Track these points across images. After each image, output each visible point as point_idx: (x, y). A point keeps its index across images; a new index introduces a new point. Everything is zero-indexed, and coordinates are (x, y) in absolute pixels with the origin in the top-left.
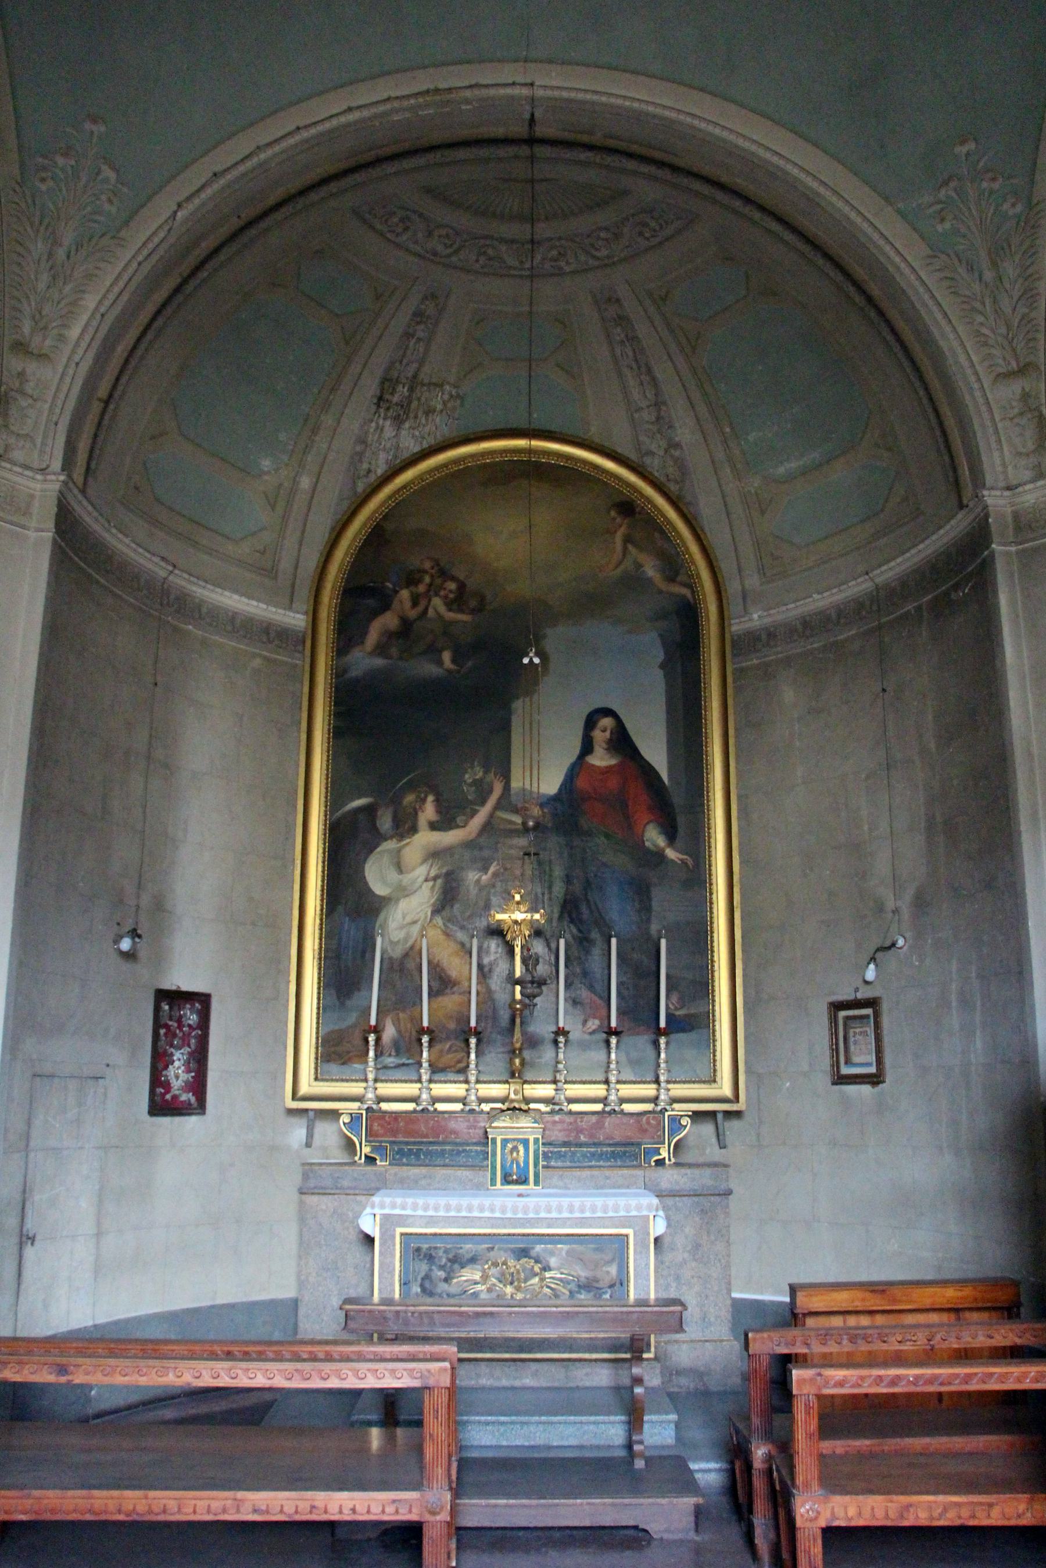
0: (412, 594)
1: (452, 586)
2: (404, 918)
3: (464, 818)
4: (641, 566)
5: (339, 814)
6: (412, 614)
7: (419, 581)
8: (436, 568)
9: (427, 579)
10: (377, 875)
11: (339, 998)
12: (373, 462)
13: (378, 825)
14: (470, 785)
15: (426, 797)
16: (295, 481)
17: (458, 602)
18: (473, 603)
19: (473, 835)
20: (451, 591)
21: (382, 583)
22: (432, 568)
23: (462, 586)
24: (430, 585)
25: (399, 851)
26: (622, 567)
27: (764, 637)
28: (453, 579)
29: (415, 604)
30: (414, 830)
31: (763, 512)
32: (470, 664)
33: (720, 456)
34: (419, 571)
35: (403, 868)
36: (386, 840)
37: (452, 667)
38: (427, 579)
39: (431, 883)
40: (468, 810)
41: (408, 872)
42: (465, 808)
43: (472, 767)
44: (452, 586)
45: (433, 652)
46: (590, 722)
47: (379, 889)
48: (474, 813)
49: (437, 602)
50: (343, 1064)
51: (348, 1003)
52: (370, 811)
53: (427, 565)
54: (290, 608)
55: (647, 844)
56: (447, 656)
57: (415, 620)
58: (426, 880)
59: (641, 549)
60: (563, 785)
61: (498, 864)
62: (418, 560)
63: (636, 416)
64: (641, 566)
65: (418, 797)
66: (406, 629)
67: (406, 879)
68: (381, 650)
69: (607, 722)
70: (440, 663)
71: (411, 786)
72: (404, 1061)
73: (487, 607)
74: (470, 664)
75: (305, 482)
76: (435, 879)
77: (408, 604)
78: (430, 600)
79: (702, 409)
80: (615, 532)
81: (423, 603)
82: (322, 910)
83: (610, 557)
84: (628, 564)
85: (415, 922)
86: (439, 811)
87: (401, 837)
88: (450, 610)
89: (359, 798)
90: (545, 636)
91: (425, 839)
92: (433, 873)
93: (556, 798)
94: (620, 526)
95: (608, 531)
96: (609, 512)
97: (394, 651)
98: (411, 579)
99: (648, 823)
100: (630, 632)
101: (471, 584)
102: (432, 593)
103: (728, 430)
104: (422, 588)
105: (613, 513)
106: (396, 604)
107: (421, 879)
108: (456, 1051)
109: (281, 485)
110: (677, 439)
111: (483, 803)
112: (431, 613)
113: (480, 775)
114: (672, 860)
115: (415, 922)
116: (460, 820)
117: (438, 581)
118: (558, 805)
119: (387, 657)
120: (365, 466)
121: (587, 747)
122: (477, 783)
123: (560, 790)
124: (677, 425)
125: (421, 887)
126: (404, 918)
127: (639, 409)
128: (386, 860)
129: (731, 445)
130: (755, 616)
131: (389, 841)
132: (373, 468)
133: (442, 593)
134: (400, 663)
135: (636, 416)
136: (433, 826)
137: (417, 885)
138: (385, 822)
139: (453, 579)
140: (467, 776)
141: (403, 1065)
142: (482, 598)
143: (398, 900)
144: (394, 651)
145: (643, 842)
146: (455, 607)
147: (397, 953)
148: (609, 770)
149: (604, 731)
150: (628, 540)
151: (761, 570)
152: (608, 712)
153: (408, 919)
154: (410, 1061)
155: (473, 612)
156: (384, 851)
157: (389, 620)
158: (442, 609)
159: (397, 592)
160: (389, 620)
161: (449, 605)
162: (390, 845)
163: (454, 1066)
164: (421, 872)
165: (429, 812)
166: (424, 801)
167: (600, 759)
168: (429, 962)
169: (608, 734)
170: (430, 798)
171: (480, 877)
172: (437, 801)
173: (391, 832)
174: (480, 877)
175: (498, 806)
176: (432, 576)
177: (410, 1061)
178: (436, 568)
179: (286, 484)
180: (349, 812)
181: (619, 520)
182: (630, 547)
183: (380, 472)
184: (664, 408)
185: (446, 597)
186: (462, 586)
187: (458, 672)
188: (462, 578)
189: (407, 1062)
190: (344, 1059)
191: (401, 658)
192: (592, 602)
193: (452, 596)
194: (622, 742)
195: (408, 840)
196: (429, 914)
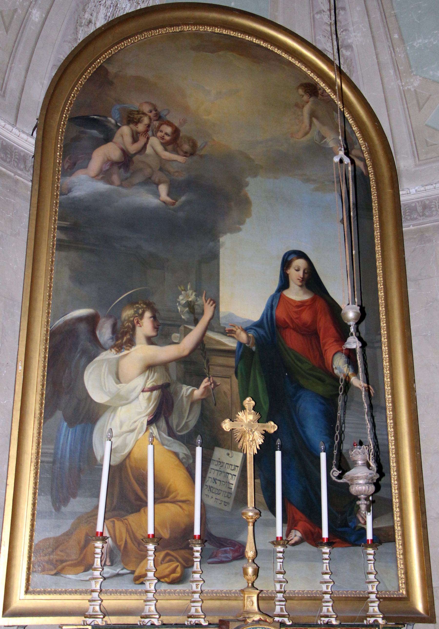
0: (132, 131)
1: (169, 130)
2: (121, 427)
3: (178, 335)
4: (323, 138)
5: (60, 321)
6: (132, 148)
7: (139, 121)
8: (154, 112)
9: (146, 120)
10: (96, 382)
11: (54, 504)
12: (95, 14)
13: (97, 333)
14: (184, 306)
15: (143, 313)
16: (27, 12)
17: (174, 142)
18: (186, 147)
19: (186, 353)
20: (166, 134)
21: (106, 117)
22: (151, 112)
23: (176, 131)
24: (149, 126)
25: (118, 361)
26: (309, 136)
27: (419, 209)
28: (169, 124)
29: (135, 140)
30: (131, 343)
31: (420, 108)
32: (183, 198)
33: (385, 57)
34: (138, 112)
35: (122, 379)
36: (106, 350)
37: (168, 199)
38: (146, 120)
39: (148, 394)
40: (182, 328)
41: (127, 382)
42: (179, 326)
43: (185, 290)
44: (169, 130)
45: (150, 183)
46: (286, 263)
47: (98, 396)
48: (187, 331)
49: (155, 142)
50: (56, 574)
51: (63, 509)
52: (92, 321)
53: (146, 108)
54: (14, 125)
55: (336, 371)
56: (163, 189)
57: (136, 154)
58: (143, 391)
59: (323, 123)
60: (265, 315)
61: (209, 380)
62: (136, 102)
63: (318, 17)
64: (323, 138)
65: (136, 312)
66: (126, 161)
67: (124, 388)
68: (104, 175)
69: (300, 263)
70: (157, 195)
71: (131, 302)
72: (118, 570)
73: (198, 153)
74: (183, 198)
75: (36, 15)
76: (152, 390)
77: (128, 139)
78: (148, 139)
79: (376, 16)
80: (303, 107)
81: (142, 141)
82: (41, 414)
83: (297, 126)
84: (313, 135)
85: (132, 431)
86: (156, 328)
87: (119, 348)
88: (166, 150)
89: (85, 307)
90: (247, 184)
91: (142, 352)
92: (149, 385)
93: (259, 325)
94: (307, 102)
95: (296, 105)
96: (297, 91)
97: (115, 178)
98: (132, 118)
99: (336, 353)
100: (317, 189)
101: (184, 131)
102: (150, 133)
103: (396, 36)
104: (141, 127)
105: (301, 91)
106: (117, 138)
107: (140, 388)
108: (170, 561)
109: (15, 11)
110: (349, 41)
111: (196, 322)
112: (149, 150)
113: (192, 298)
114: (358, 388)
115: (132, 431)
116: (175, 336)
117: (156, 123)
118: (261, 332)
119: (110, 182)
120: (87, 16)
121: (285, 283)
122: (190, 306)
123: (262, 319)
124: (351, 29)
125: (137, 397)
126: (121, 427)
127: (321, 12)
128: (105, 369)
129: (397, 50)
130: (413, 191)
131: (108, 351)
132: (93, 19)
133: (159, 134)
134: (120, 189)
135: (318, 17)
136: (150, 341)
137: (134, 394)
138: (105, 333)
139: (169, 124)
140: (181, 297)
141: (118, 575)
142: (194, 145)
143: (115, 409)
144: (115, 178)
145: (333, 369)
146: (170, 147)
147: (117, 460)
148: (302, 304)
149: (298, 270)
150: (313, 115)
151: (416, 154)
152: (301, 255)
153: (125, 428)
154: (125, 571)
155: (185, 154)
156: (103, 361)
157: (110, 151)
158: (160, 148)
159: (119, 127)
160: (110, 151)
161: (165, 145)
162: (108, 355)
163: (167, 576)
164: (139, 382)
165: (146, 327)
166: (141, 316)
167: (296, 294)
168: (134, 477)
169: (301, 273)
170: (148, 314)
171: (193, 391)
172: (154, 317)
173: (110, 343)
174: (193, 391)
175: (209, 327)
176: (150, 119)
177: (125, 571)
178: (154, 112)
179: (19, 11)
180: (71, 320)
181: (306, 98)
182: (314, 120)
183: (99, 25)
184: (342, 13)
185: (162, 138)
186: (176, 131)
187: (173, 204)
188: (177, 124)
189: (122, 572)
190: (58, 568)
191: (121, 185)
192: (283, 162)
193: (167, 138)
194: (312, 281)
195: (126, 352)
196: (145, 423)
